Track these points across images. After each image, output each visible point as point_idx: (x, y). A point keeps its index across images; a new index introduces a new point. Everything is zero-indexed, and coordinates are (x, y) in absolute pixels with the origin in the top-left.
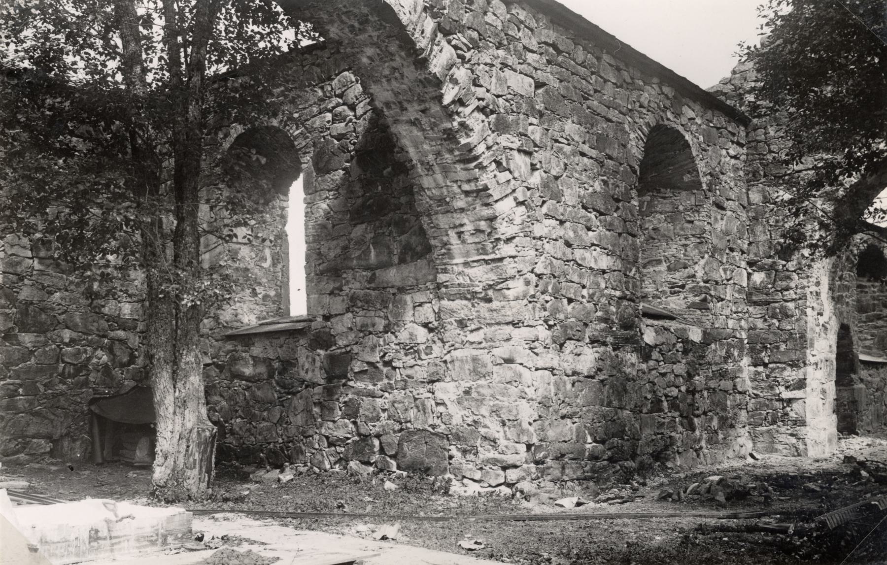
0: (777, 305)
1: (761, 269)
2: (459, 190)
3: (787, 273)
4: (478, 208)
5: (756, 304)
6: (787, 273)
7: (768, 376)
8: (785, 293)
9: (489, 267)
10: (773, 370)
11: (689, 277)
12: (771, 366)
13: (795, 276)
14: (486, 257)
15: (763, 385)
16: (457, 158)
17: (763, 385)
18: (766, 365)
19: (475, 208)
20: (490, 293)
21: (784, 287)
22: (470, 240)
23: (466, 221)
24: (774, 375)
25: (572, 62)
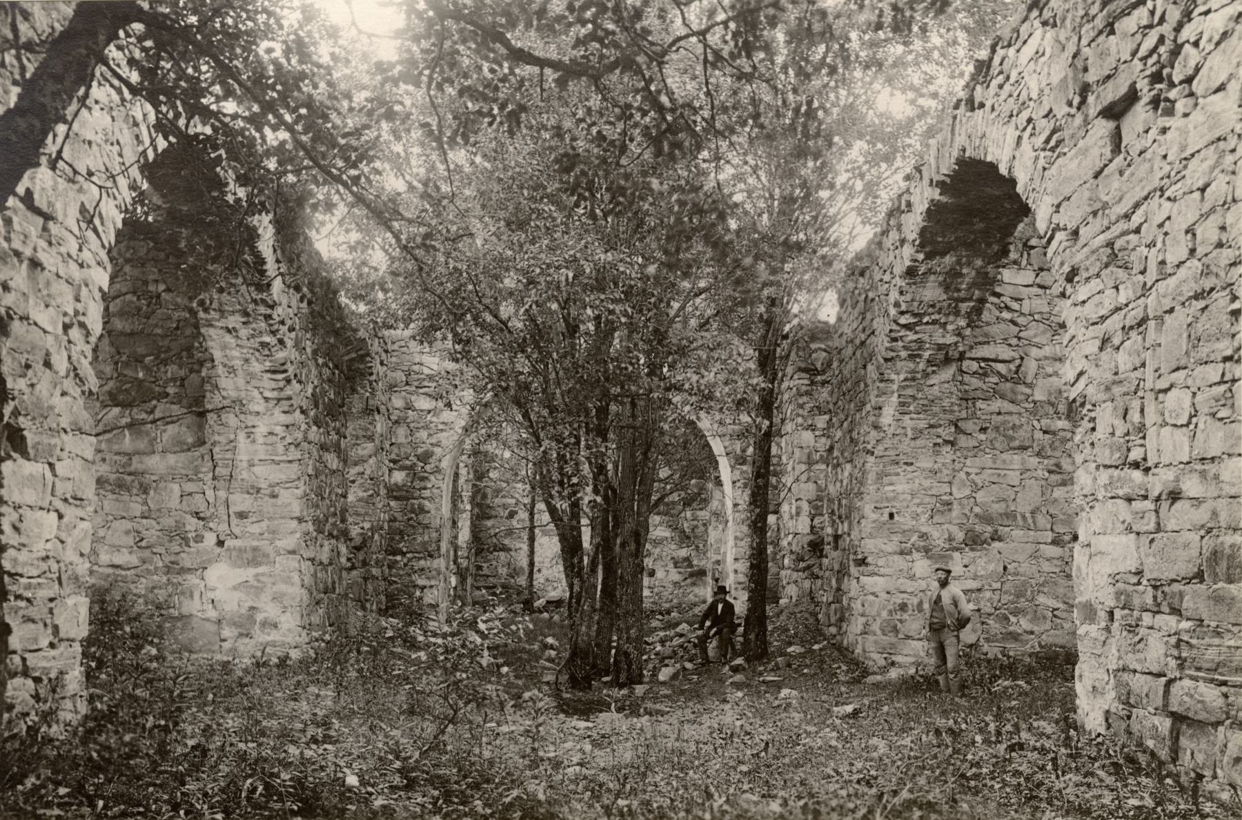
5: (396, 498)
7: (405, 565)
10: (410, 560)
18: (404, 554)
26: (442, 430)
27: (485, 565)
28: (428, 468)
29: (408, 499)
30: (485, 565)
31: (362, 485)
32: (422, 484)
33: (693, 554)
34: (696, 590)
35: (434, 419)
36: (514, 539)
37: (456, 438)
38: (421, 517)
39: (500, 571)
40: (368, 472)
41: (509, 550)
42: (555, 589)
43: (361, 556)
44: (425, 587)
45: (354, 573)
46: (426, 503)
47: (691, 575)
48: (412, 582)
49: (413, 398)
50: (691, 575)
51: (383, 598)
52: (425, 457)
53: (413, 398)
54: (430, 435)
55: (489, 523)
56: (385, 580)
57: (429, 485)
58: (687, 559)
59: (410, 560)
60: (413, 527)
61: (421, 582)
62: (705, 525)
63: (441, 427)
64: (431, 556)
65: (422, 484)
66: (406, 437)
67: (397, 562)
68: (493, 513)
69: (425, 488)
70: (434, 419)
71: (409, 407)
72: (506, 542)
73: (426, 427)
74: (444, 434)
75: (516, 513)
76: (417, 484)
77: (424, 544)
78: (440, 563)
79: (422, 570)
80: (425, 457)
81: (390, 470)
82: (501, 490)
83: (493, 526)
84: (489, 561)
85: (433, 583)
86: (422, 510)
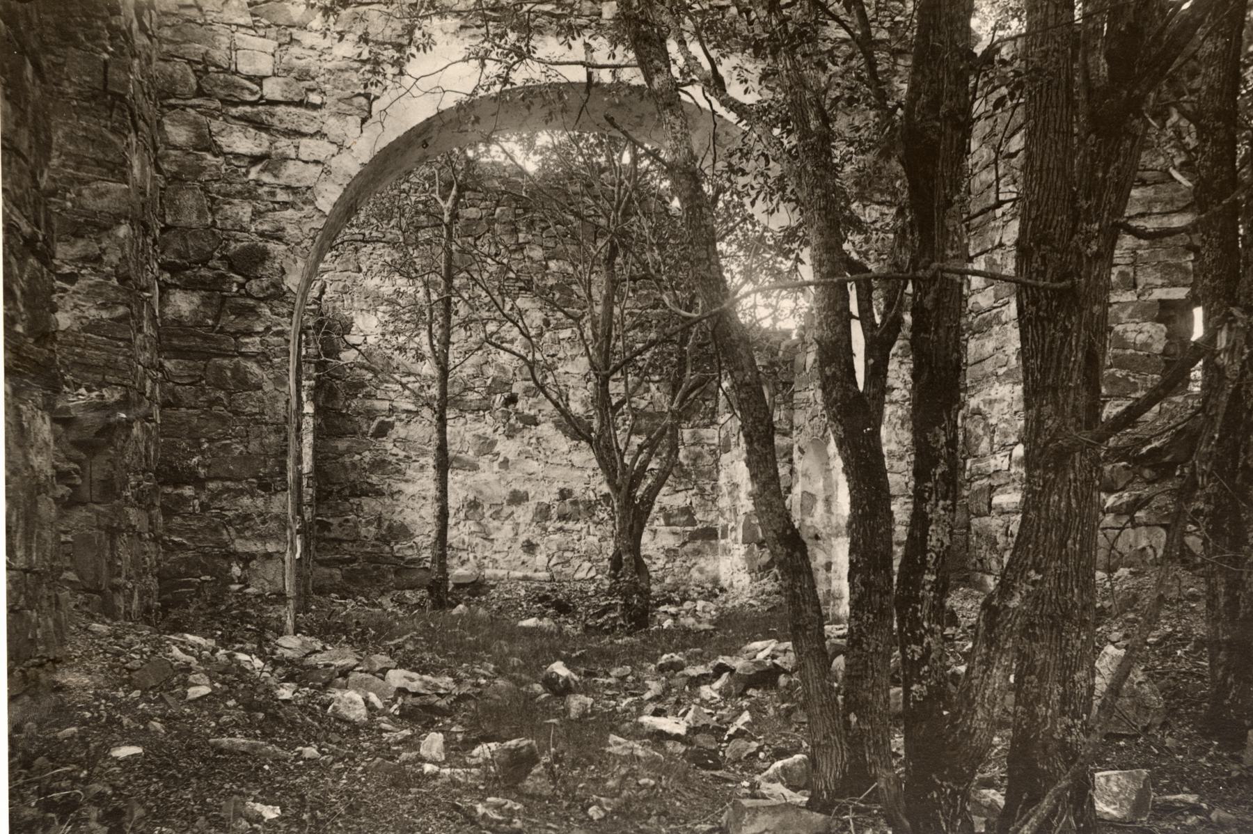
0: (226, 362)
5: (179, 353)
6: (251, 302)
7: (205, 507)
10: (215, 496)
11: (85, 259)
12: (211, 485)
15: (195, 524)
18: (199, 483)
21: (242, 327)
24: (218, 504)
26: (285, 205)
27: (334, 521)
28: (254, 286)
29: (208, 356)
30: (334, 521)
31: (93, 292)
32: (242, 324)
33: (696, 501)
34: (702, 562)
35: (267, 178)
36: (389, 475)
37: (319, 224)
38: (240, 397)
39: (363, 531)
40: (113, 257)
41: (379, 493)
42: (463, 563)
43: (99, 468)
44: (252, 556)
45: (79, 514)
46: (253, 367)
47: (694, 537)
48: (222, 544)
49: (215, 125)
50: (694, 537)
51: (152, 583)
52: (252, 260)
53: (215, 125)
54: (257, 214)
55: (342, 445)
56: (155, 540)
57: (260, 328)
58: (687, 511)
59: (215, 496)
60: (223, 420)
61: (240, 546)
62: (713, 452)
63: (282, 196)
64: (266, 487)
65: (242, 324)
66: (201, 214)
67: (184, 500)
68: (349, 426)
69: (249, 333)
70: (267, 178)
71: (206, 142)
72: (374, 479)
73: (249, 194)
74: (289, 213)
75: (391, 425)
76: (230, 321)
77: (247, 458)
78: (282, 503)
79: (246, 517)
80: (252, 260)
81: (165, 288)
82: (362, 385)
83: (349, 451)
84: (342, 514)
85: (271, 547)
86: (243, 382)
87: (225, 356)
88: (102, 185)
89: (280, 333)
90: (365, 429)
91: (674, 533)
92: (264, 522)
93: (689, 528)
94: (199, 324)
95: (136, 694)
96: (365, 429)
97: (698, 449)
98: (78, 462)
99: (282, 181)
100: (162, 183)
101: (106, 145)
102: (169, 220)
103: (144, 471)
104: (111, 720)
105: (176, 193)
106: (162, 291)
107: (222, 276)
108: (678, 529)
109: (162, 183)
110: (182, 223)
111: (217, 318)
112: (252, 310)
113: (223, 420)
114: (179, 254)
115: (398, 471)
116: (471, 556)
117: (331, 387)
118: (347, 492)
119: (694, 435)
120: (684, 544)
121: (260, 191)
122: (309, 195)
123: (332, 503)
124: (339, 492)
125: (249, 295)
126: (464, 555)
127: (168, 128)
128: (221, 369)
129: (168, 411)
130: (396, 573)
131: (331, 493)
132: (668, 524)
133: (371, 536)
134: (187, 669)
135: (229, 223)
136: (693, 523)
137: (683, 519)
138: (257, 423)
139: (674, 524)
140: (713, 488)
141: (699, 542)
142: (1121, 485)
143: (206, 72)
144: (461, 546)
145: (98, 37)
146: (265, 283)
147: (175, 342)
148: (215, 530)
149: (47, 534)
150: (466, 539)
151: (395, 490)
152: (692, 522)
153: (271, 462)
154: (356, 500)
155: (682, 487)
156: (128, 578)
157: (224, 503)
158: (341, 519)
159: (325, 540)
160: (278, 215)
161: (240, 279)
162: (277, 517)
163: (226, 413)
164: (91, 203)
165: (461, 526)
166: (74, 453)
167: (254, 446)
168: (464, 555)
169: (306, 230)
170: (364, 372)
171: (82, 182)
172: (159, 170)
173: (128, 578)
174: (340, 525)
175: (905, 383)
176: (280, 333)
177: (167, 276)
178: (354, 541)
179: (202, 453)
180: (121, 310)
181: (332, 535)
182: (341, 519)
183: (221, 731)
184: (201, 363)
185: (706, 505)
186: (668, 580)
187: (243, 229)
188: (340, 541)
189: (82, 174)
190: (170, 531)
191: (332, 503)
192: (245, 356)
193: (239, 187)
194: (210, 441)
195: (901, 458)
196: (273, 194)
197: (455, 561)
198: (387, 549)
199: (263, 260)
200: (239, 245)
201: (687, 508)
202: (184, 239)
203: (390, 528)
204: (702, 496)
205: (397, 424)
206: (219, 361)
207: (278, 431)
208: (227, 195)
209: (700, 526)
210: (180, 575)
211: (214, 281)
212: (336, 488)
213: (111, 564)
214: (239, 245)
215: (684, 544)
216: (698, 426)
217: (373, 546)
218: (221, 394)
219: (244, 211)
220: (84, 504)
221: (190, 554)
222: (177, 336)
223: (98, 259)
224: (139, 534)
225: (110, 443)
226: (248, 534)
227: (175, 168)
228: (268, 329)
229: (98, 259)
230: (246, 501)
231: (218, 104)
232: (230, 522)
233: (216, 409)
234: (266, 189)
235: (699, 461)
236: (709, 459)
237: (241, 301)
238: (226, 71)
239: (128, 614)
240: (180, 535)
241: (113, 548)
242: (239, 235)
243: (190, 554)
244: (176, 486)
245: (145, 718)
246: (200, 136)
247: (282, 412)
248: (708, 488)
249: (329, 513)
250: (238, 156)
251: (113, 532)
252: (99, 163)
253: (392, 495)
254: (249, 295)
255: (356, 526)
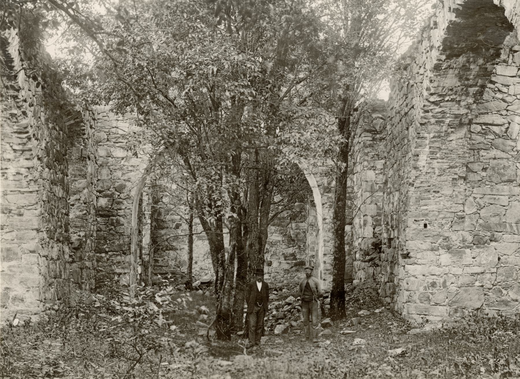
0: (114, 218)
1: (105, 196)
2: (10, 148)
3: (121, 200)
4: (21, 161)
5: (102, 216)
6: (121, 200)
7: (108, 259)
8: (119, 211)
9: (23, 195)
10: (111, 256)
11: (76, 200)
12: (110, 253)
13: (125, 202)
14: (22, 190)
15: (105, 264)
16: (16, 131)
17: (105, 264)
18: (106, 253)
19: (19, 161)
20: (22, 210)
21: (119, 208)
22: (11, 178)
23: (10, 167)
24: (111, 259)
25: (395, 166)
28: (122, 196)
29: (109, 216)
33: (297, 251)
35: (126, 163)
38: (118, 228)
39: (170, 263)
40: (83, 199)
41: (176, 249)
42: (206, 275)
47: (296, 265)
48: (112, 270)
51: (93, 281)
54: (123, 174)
56: (94, 269)
57: (123, 207)
58: (293, 255)
59: (111, 256)
60: (113, 235)
62: (304, 232)
63: (130, 168)
64: (125, 254)
66: (108, 175)
67: (102, 257)
68: (166, 225)
69: (120, 209)
70: (126, 163)
71: (109, 156)
72: (174, 244)
73: (121, 169)
74: (133, 173)
75: (181, 225)
76: (115, 206)
77: (120, 245)
79: (119, 262)
83: (165, 234)
84: (163, 256)
85: (126, 271)
87: (114, 216)
88: (80, 181)
89: (129, 209)
90: (171, 226)
91: (288, 263)
92: (124, 264)
93: (294, 261)
94: (107, 207)
95: (84, 305)
96: (171, 226)
97: (298, 231)
98: (74, 252)
99: (131, 164)
100: (97, 167)
101: (81, 170)
102: (99, 178)
103: (90, 251)
104: (79, 310)
105: (101, 169)
106: (97, 198)
107: (113, 193)
108: (290, 262)
109: (97, 167)
110: (103, 178)
111: (112, 205)
112: (121, 202)
113: (113, 235)
114: (102, 187)
115: (183, 241)
116: (209, 272)
117: (159, 211)
118: (165, 249)
119: (296, 226)
120: (292, 267)
121: (124, 167)
122: (138, 168)
123: (159, 253)
124: (162, 249)
125: (120, 198)
126: (207, 272)
127: (99, 151)
128: (112, 220)
129: (98, 232)
130: (182, 278)
131: (159, 249)
132: (285, 260)
133: (173, 265)
134: (96, 301)
135: (115, 178)
136: (296, 259)
137: (292, 258)
138: (122, 235)
139: (288, 260)
140: (304, 246)
141: (298, 267)
142: (370, 253)
143: (110, 134)
144: (205, 268)
145: (80, 142)
146: (125, 194)
147: (100, 212)
148: (111, 266)
149: (68, 271)
150: (208, 265)
151: (182, 247)
152: (295, 259)
153: (126, 246)
154: (168, 252)
155: (291, 246)
156: (86, 280)
157: (113, 258)
158: (162, 259)
159: (157, 266)
160: (129, 174)
161: (119, 194)
162: (128, 262)
163: (114, 233)
164: (78, 186)
165: (206, 261)
166: (73, 250)
167: (121, 242)
168: (207, 272)
169: (137, 178)
170: (171, 206)
171: (76, 181)
172: (97, 163)
173: (86, 280)
174: (162, 261)
175: (330, 217)
176: (129, 209)
177: (98, 194)
178: (167, 266)
179: (107, 244)
180: (85, 212)
181: (159, 264)
182: (162, 259)
183: (100, 313)
184: (107, 219)
185: (301, 252)
186: (285, 282)
187: (119, 179)
188: (162, 266)
189: (76, 179)
190: (98, 266)
191: (159, 253)
192: (120, 216)
193: (118, 167)
194: (110, 241)
195: (328, 242)
196: (128, 168)
197: (203, 274)
198: (179, 269)
199: (124, 188)
200: (118, 184)
201: (293, 254)
202: (103, 183)
203: (180, 262)
204: (300, 249)
205: (183, 224)
206: (112, 218)
207: (128, 237)
208: (115, 169)
209: (298, 260)
210: (101, 279)
211: (111, 195)
212: (161, 247)
213: (81, 277)
214: (118, 184)
215: (292, 267)
216: (298, 222)
217: (174, 268)
218: (113, 227)
219: (119, 174)
220: (75, 262)
221: (104, 273)
222: (101, 211)
223: (79, 199)
224: (89, 268)
225: (81, 247)
226: (119, 267)
227: (101, 163)
228: (126, 208)
229: (79, 199)
230: (119, 257)
231: (113, 143)
232: (115, 264)
233: (111, 232)
234: (126, 167)
235: (298, 236)
236: (302, 235)
237: (118, 200)
238: (115, 134)
239: (85, 290)
240: (101, 267)
241: (82, 272)
242: (118, 181)
243: (104, 273)
244: (100, 253)
245: (85, 310)
246: (108, 153)
247: (130, 232)
248: (302, 246)
249: (158, 256)
250: (118, 158)
251: (81, 269)
252: (80, 175)
253: (181, 249)
254: (120, 198)
255: (167, 261)
